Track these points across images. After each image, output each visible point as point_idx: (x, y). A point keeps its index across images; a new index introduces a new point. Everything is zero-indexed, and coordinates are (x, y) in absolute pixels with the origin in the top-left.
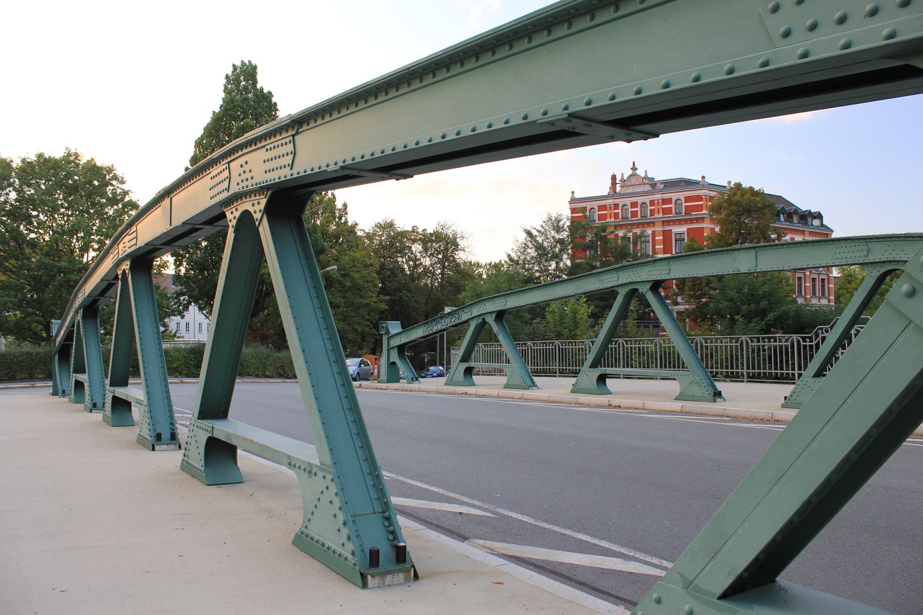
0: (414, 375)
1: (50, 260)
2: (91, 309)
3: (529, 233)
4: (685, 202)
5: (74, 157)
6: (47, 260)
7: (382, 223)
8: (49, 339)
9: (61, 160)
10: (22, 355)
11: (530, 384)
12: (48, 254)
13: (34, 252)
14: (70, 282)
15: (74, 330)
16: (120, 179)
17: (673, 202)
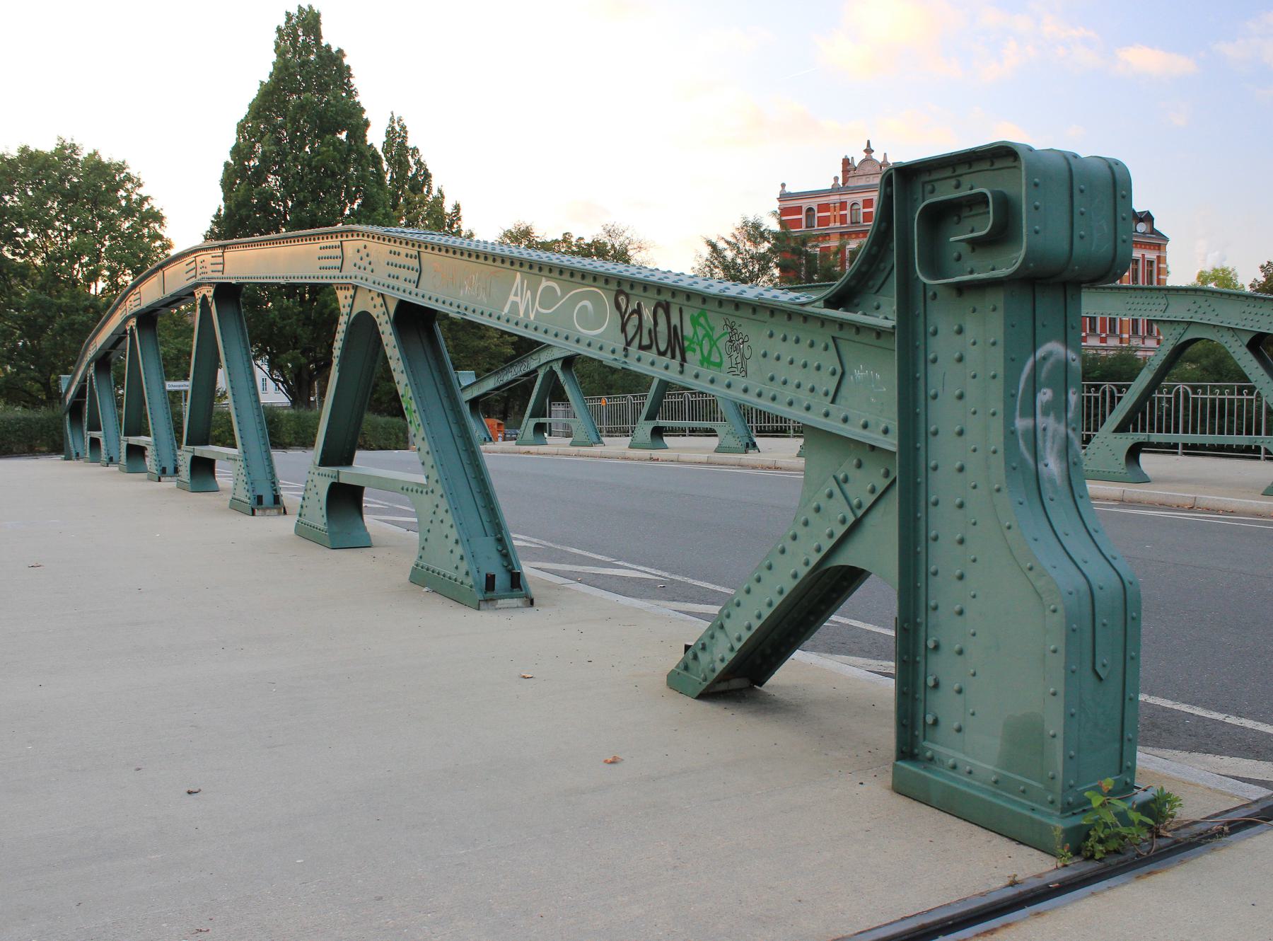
0: (488, 435)
1: (47, 295)
2: (103, 362)
3: (714, 246)
4: (818, 212)
5: (70, 151)
6: (43, 296)
7: (513, 231)
8: (59, 397)
9: (53, 154)
10: (18, 421)
11: (595, 439)
12: (42, 288)
13: (24, 285)
14: (74, 325)
15: (86, 385)
16: (136, 180)
17: (849, 207)
